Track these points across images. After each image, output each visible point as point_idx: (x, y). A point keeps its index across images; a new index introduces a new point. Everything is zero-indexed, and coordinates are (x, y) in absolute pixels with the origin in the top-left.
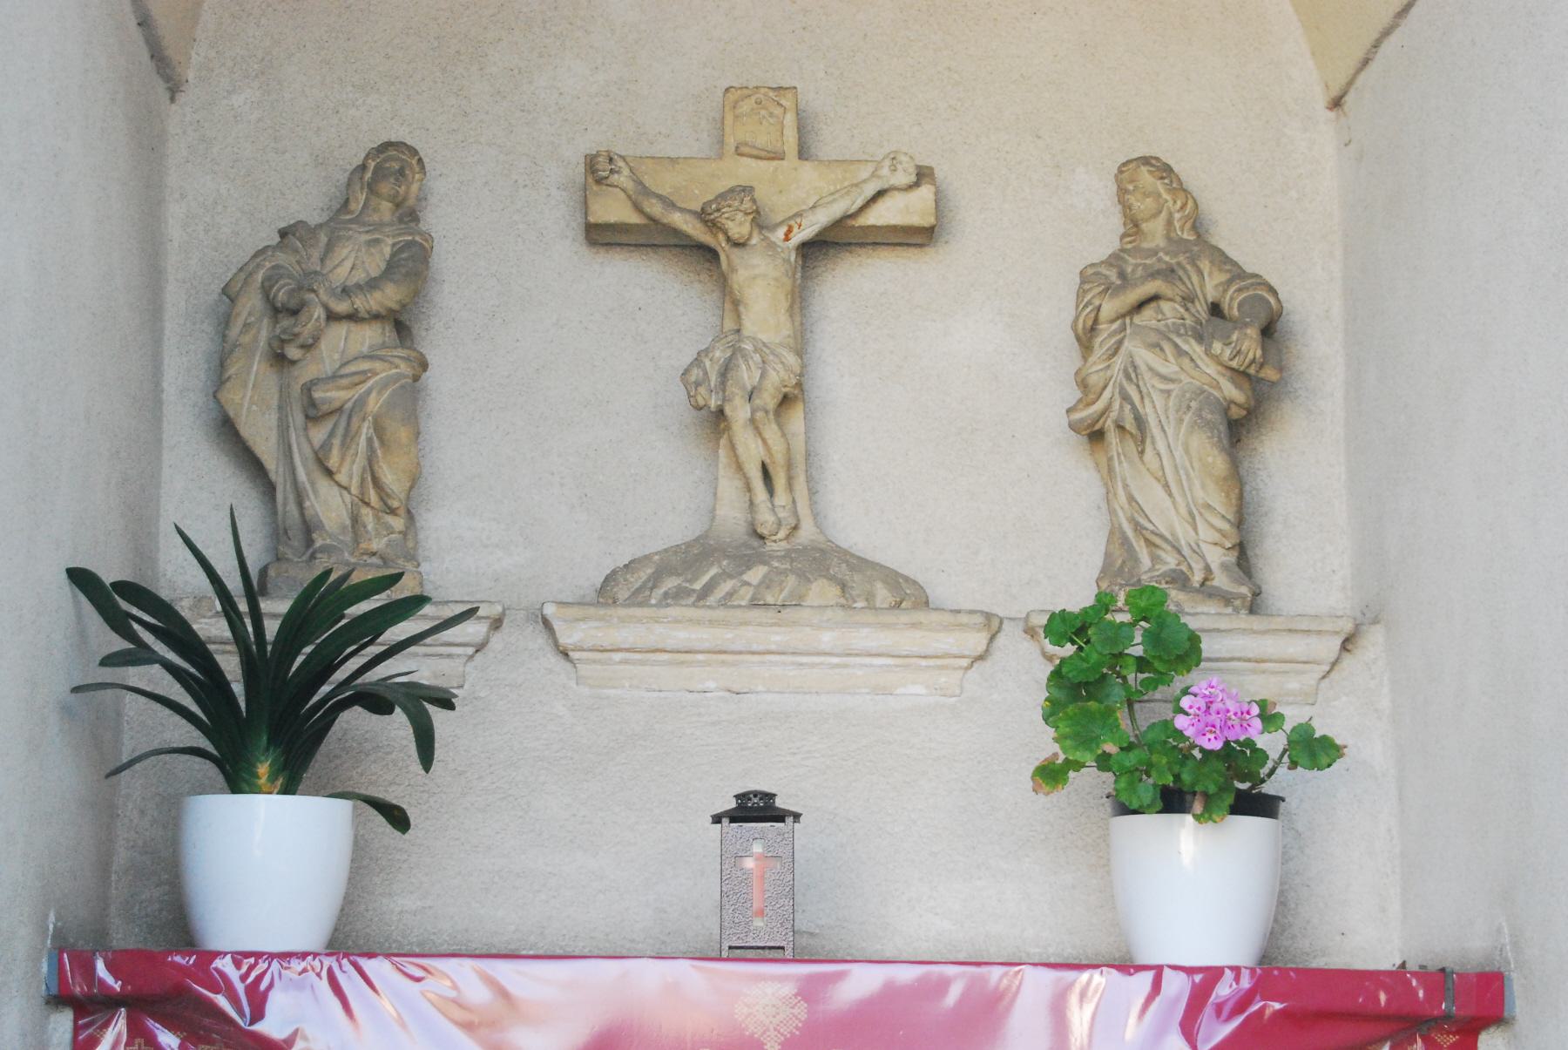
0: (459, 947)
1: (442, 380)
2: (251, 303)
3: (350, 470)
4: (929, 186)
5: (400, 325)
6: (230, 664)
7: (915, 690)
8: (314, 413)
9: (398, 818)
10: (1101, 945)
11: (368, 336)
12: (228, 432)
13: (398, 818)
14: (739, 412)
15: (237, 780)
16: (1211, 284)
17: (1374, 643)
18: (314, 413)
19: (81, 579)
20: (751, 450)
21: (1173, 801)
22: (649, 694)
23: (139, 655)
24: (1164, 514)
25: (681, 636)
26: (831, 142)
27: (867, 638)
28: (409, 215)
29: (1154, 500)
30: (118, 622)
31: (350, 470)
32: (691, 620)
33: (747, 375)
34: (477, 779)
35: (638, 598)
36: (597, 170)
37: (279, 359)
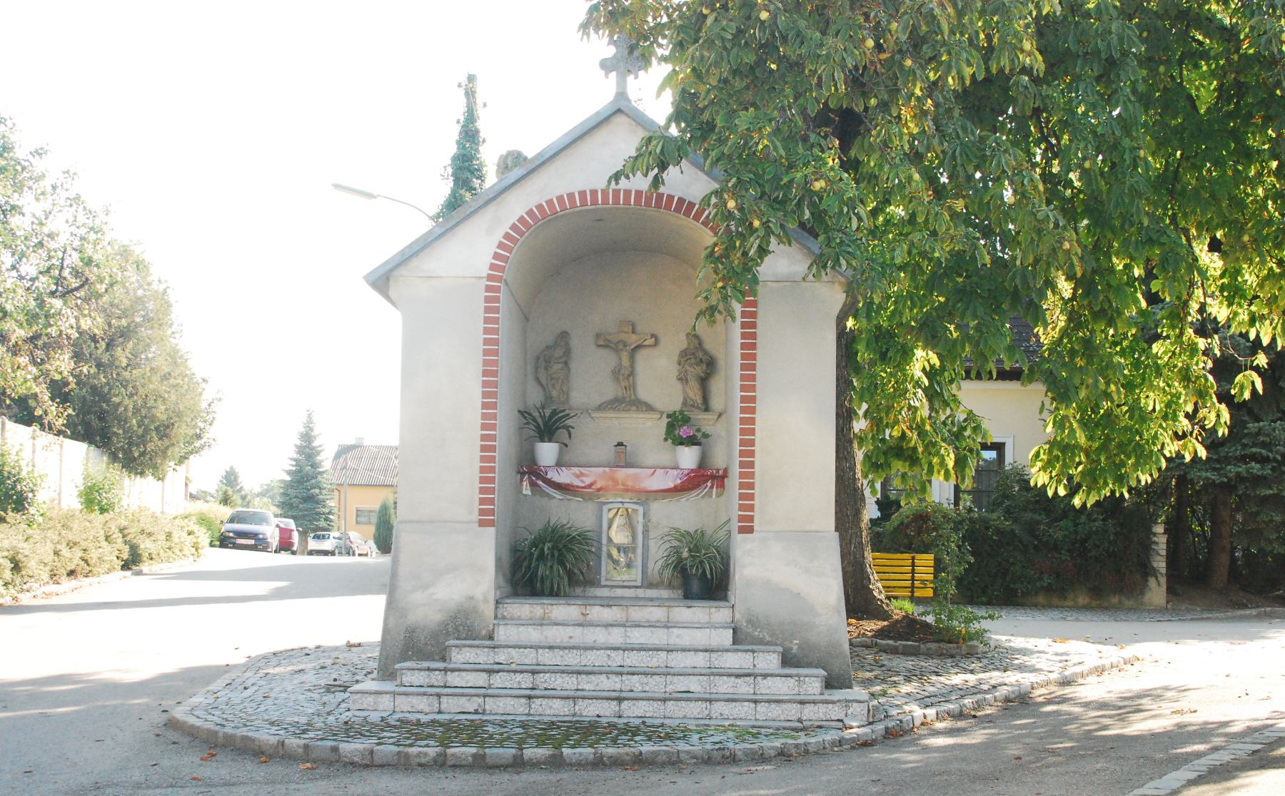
0: (471, 705)
1: (573, 370)
2: (541, 359)
3: (558, 387)
4: (450, 652)
5: (566, 363)
6: (541, 423)
7: (649, 424)
8: (552, 379)
9: (566, 446)
10: (672, 465)
11: (560, 366)
12: (537, 379)
13: (566, 446)
14: (621, 378)
15: (543, 441)
16: (700, 355)
17: (723, 417)
18: (552, 379)
19: (519, 411)
20: (623, 384)
21: (681, 444)
22: (300, 668)
23: (528, 423)
24: (691, 395)
25: (611, 415)
26: (639, 328)
27: (641, 415)
28: (567, 344)
29: (689, 391)
30: (525, 418)
31: (558, 387)
32: (290, 758)
33: (622, 372)
34: (107, 349)
35: (604, 409)
36: (598, 336)
37: (546, 368)
